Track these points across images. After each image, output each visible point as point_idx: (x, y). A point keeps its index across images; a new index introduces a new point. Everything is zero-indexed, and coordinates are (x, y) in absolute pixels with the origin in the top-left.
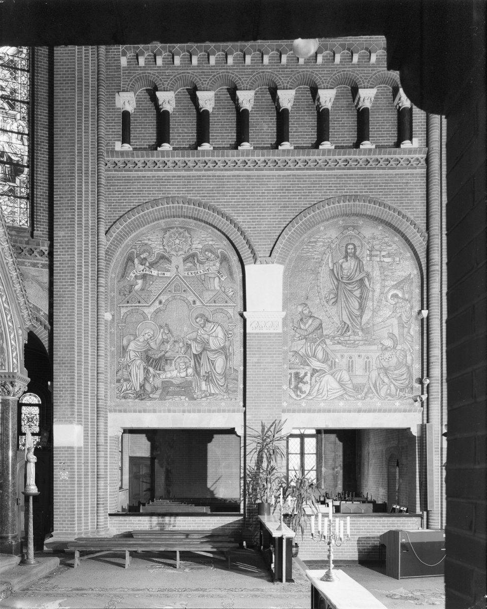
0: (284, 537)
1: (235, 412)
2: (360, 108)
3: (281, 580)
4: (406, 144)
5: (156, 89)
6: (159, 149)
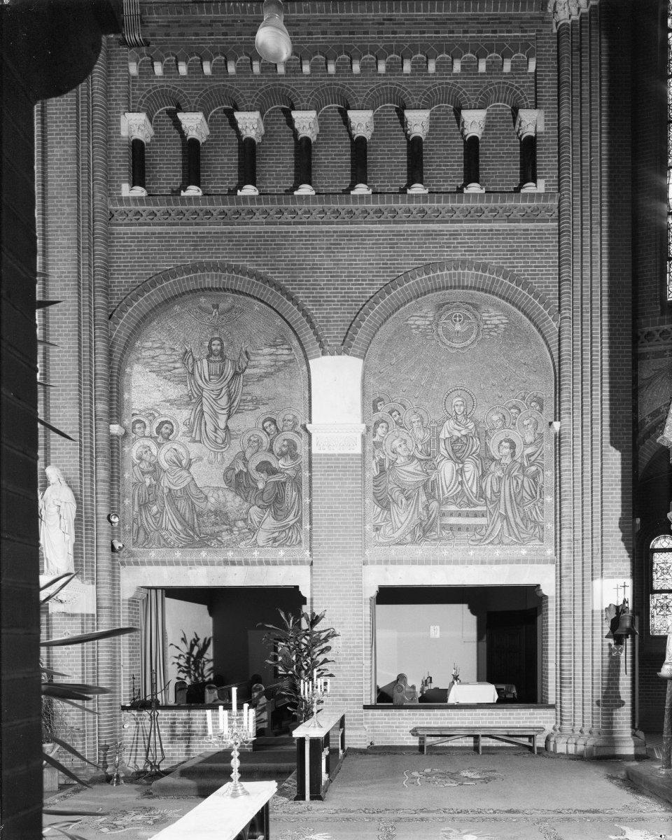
0: (307, 739)
1: (437, 564)
2: (521, 136)
3: (303, 798)
4: (529, 188)
5: (404, 108)
6: (183, 194)
